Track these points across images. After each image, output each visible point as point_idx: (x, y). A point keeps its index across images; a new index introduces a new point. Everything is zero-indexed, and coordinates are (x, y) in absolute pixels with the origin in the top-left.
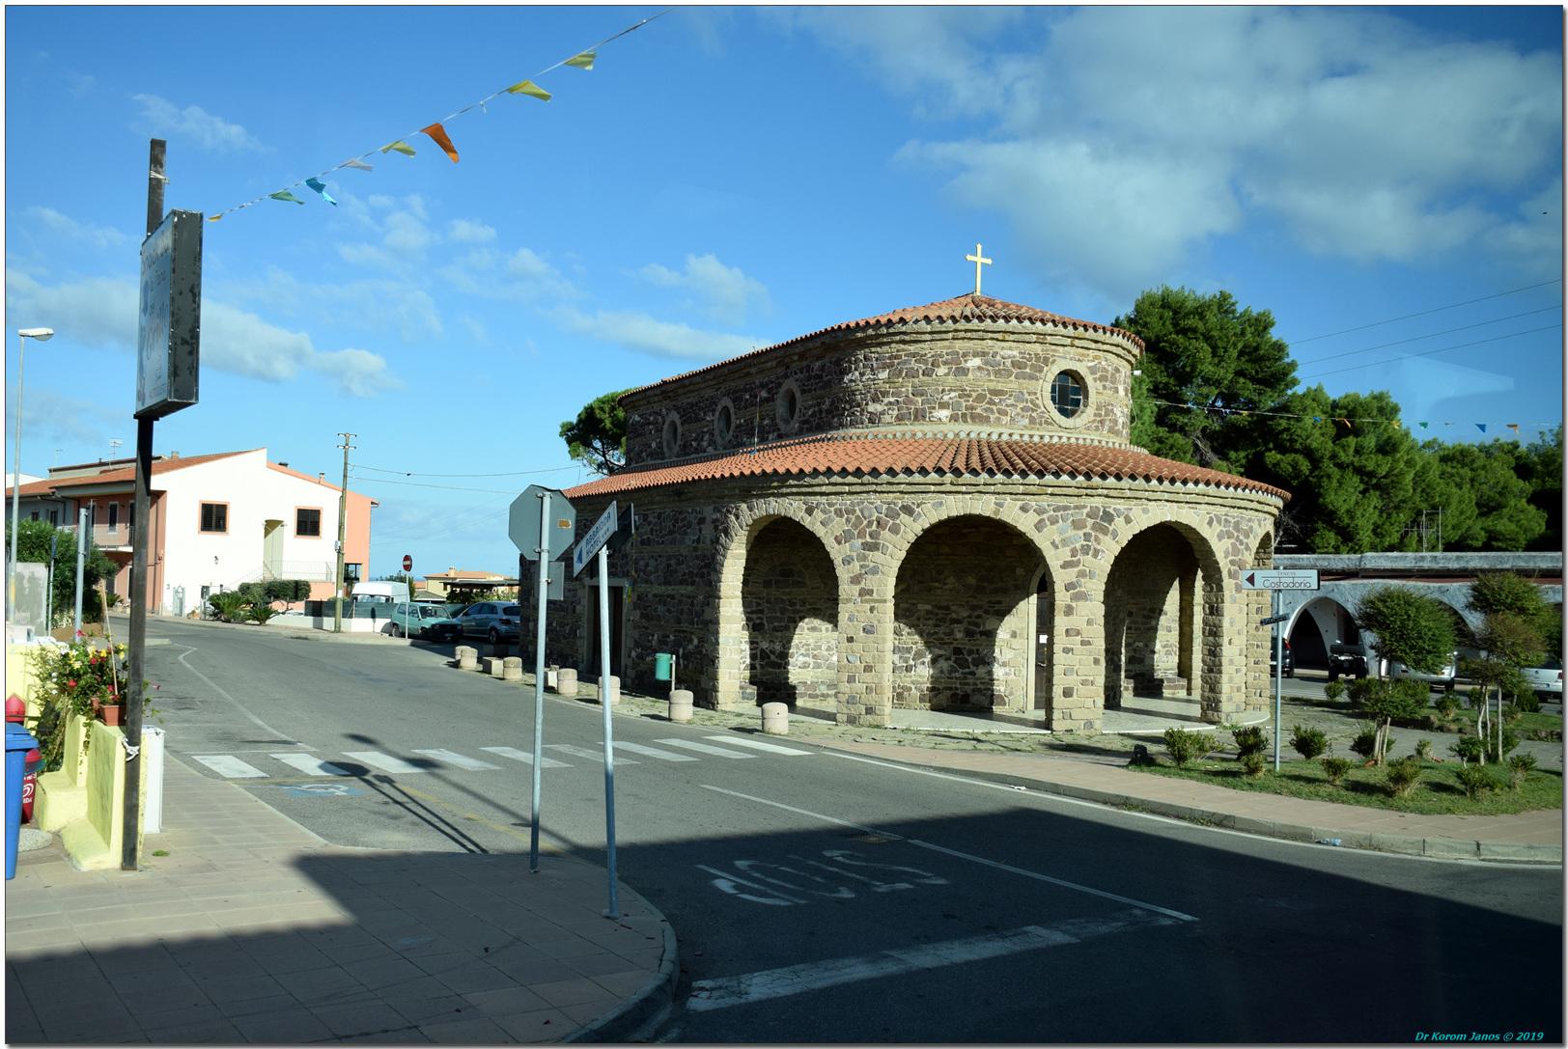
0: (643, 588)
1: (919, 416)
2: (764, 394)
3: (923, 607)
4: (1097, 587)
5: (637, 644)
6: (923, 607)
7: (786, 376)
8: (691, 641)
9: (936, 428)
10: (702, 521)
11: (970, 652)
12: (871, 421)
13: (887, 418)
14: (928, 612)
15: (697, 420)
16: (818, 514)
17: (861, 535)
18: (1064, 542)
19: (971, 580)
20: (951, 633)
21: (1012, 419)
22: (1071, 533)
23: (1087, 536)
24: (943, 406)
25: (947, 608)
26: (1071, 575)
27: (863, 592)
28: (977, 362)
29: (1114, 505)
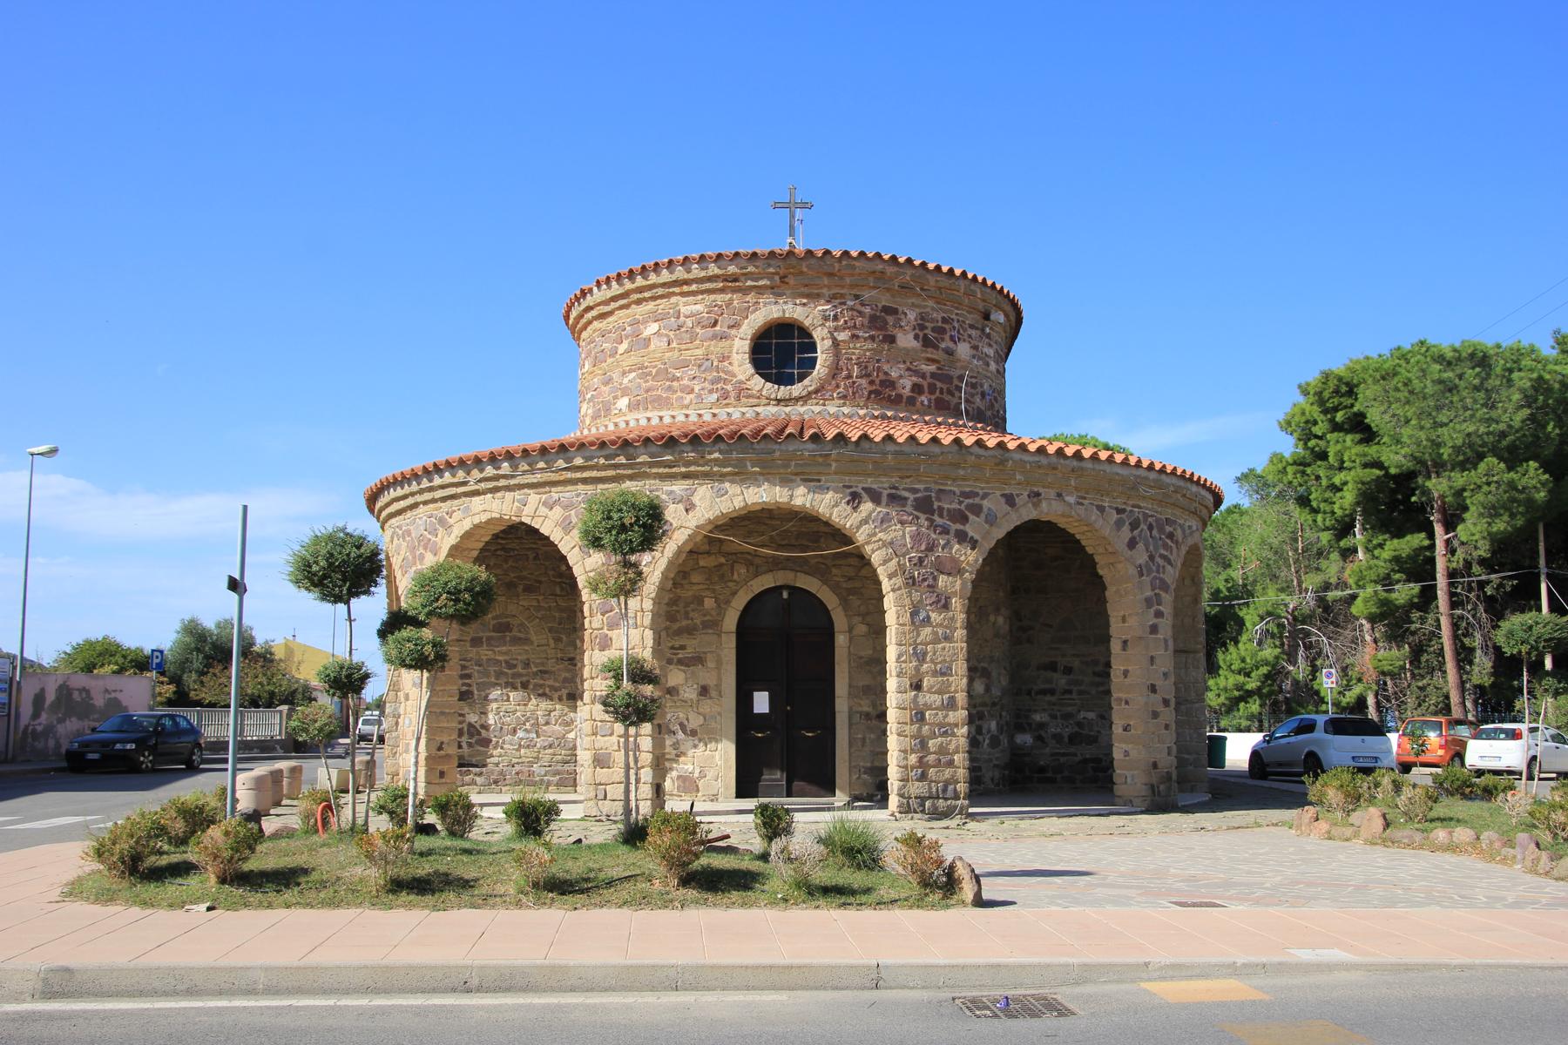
28: (653, 328)
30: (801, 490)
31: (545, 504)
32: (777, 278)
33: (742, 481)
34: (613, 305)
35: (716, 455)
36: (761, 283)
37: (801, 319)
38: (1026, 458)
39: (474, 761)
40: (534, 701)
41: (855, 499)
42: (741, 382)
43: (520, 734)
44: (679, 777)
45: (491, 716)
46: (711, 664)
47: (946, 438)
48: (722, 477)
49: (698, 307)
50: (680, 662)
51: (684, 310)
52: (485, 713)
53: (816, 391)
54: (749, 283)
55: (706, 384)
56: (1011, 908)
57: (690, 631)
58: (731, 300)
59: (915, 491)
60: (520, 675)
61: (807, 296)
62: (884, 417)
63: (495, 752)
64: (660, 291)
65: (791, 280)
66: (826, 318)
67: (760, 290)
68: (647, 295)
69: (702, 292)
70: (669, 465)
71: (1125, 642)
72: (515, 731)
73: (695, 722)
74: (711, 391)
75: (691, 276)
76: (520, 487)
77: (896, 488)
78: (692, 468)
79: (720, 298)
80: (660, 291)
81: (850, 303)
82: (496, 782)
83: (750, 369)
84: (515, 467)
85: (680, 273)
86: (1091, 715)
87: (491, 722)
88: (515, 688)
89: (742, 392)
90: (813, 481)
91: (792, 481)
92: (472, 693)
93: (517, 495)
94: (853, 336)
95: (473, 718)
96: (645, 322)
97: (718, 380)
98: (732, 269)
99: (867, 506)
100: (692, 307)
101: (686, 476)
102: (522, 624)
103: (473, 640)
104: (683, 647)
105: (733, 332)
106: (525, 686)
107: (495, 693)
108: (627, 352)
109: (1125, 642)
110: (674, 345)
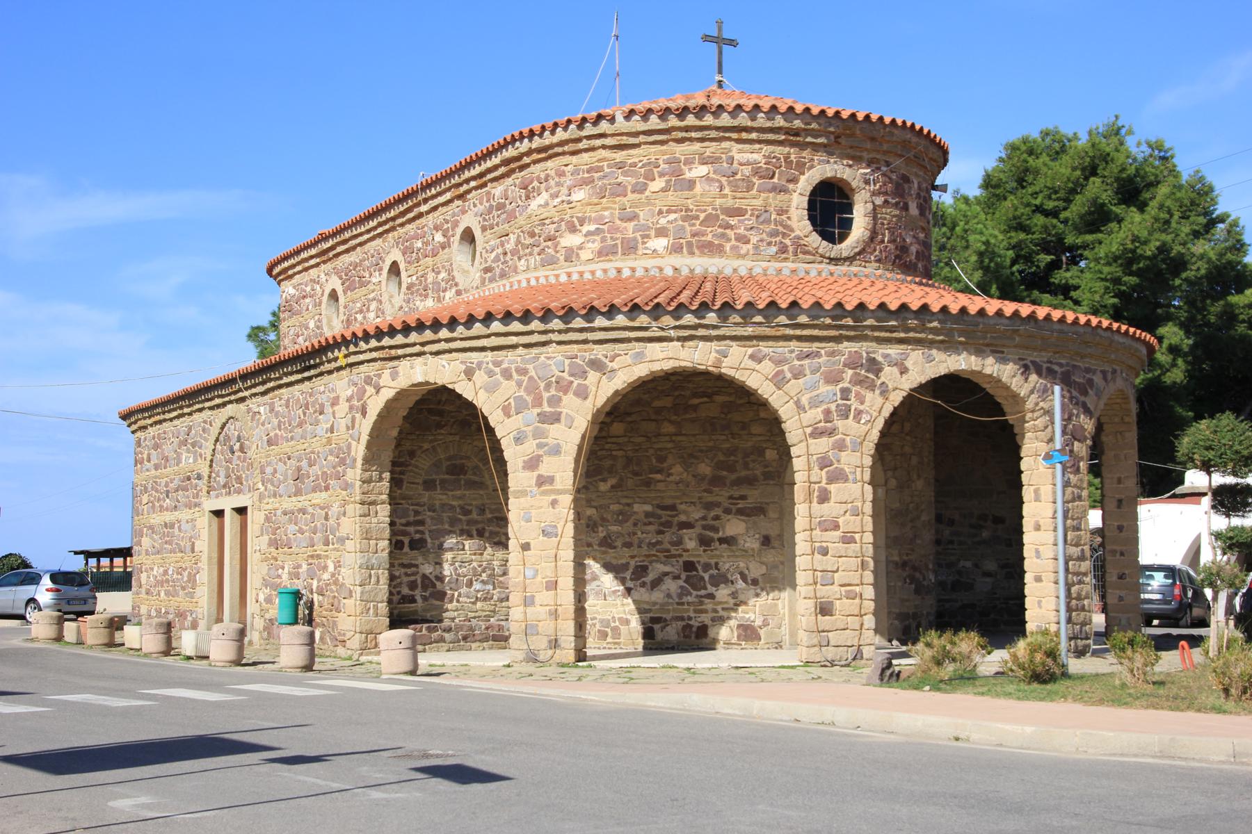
0: (272, 503)
1: (630, 248)
2: (439, 237)
3: (640, 508)
4: (858, 461)
5: (266, 584)
6: (640, 508)
7: (464, 212)
8: (325, 568)
9: (650, 263)
10: (335, 402)
11: (707, 567)
12: (568, 259)
13: (585, 255)
14: (647, 515)
15: (363, 285)
16: (480, 377)
17: (538, 402)
18: (814, 403)
19: (705, 469)
20: (679, 542)
21: (756, 247)
22: (824, 389)
23: (845, 393)
24: (662, 232)
25: (673, 508)
26: (822, 445)
27: (542, 481)
28: (703, 170)
29: (882, 352)
30: (990, 360)
31: (752, 357)
32: (832, 137)
33: (946, 350)
34: (642, 138)
35: (935, 324)
36: (819, 140)
37: (849, 180)
38: (1064, 328)
39: (428, 615)
40: (489, 550)
41: (1026, 370)
42: (799, 238)
43: (477, 586)
44: (739, 626)
45: (446, 566)
46: (772, 515)
47: (1070, 316)
48: (931, 344)
49: (755, 156)
50: (741, 512)
51: (737, 157)
52: (439, 564)
53: (859, 253)
54: (809, 139)
55: (764, 236)
56: (477, 789)
57: (751, 481)
58: (789, 153)
59: (1061, 365)
60: (476, 522)
61: (852, 158)
62: (920, 284)
63: (449, 606)
64: (713, 134)
65: (843, 141)
66: (867, 182)
67: (815, 147)
68: (693, 135)
69: (759, 142)
70: (892, 330)
71: (1120, 501)
72: (470, 584)
73: (756, 570)
74: (769, 244)
75: (755, 124)
76: (724, 338)
77: (1050, 362)
78: (912, 335)
79: (779, 151)
80: (713, 134)
81: (884, 169)
82: (465, 638)
83: (808, 226)
84: (724, 319)
85: (743, 119)
86: (968, 564)
87: (446, 573)
88: (470, 536)
89: (800, 248)
90: (1001, 355)
91: (984, 351)
92: (425, 541)
93: (714, 345)
94: (886, 202)
95: (427, 569)
96: (689, 162)
97: (774, 234)
98: (797, 123)
99: (1033, 377)
100: (748, 156)
101: (901, 341)
102: (477, 467)
103: (425, 482)
104: (743, 498)
105: (791, 186)
106: (480, 534)
107: (451, 541)
108: (664, 190)
109: (1120, 501)
110: (727, 191)
